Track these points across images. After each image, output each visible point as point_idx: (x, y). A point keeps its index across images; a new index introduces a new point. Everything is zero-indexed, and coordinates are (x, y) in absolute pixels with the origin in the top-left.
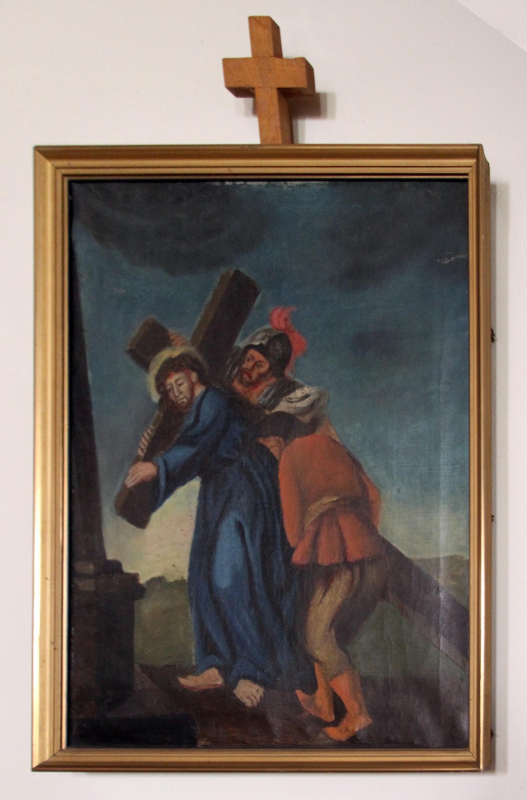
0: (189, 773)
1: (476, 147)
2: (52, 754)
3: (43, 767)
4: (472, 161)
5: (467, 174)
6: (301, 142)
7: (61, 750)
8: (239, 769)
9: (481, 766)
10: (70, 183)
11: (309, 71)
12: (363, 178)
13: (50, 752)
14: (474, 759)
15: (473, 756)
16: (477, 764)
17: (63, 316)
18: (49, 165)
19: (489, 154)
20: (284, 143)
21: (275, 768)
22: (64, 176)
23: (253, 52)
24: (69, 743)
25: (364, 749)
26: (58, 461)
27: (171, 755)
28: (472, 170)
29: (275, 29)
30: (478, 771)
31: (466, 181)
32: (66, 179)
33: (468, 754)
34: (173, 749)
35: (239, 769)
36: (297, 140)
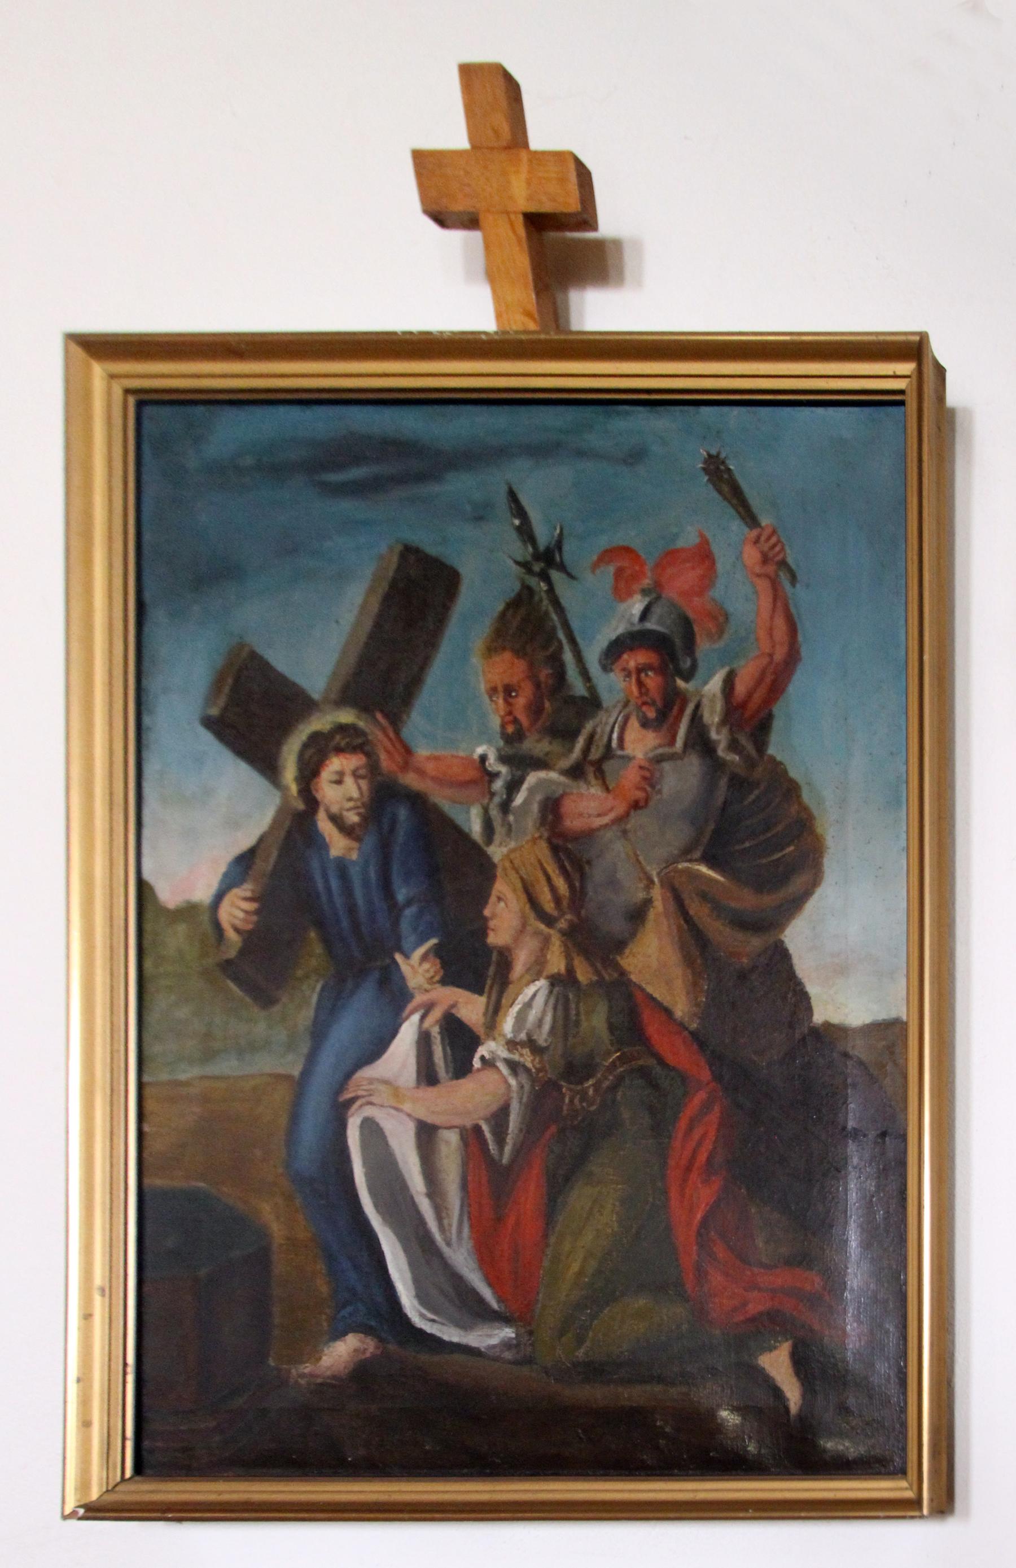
0: (468, 1522)
1: (917, 338)
2: (104, 1489)
3: (94, 1511)
4: (907, 368)
5: (902, 392)
6: (575, 326)
7: (123, 1479)
8: (134, 1515)
9: (925, 1511)
10: (140, 405)
11: (584, 176)
12: (773, 340)
13: (101, 1485)
14: (910, 1494)
15: (911, 1489)
16: (916, 1503)
17: (126, 694)
18: (98, 370)
19: (940, 350)
20: (544, 329)
21: (215, 1513)
22: (127, 391)
23: (471, 139)
24: (139, 1468)
25: (735, 1477)
26: (909, 483)
27: (404, 1489)
28: (911, 382)
29: (512, 89)
30: (922, 1517)
31: (902, 403)
32: (131, 400)
33: (904, 1484)
34: (477, 1478)
35: (134, 1515)
36: (567, 321)
